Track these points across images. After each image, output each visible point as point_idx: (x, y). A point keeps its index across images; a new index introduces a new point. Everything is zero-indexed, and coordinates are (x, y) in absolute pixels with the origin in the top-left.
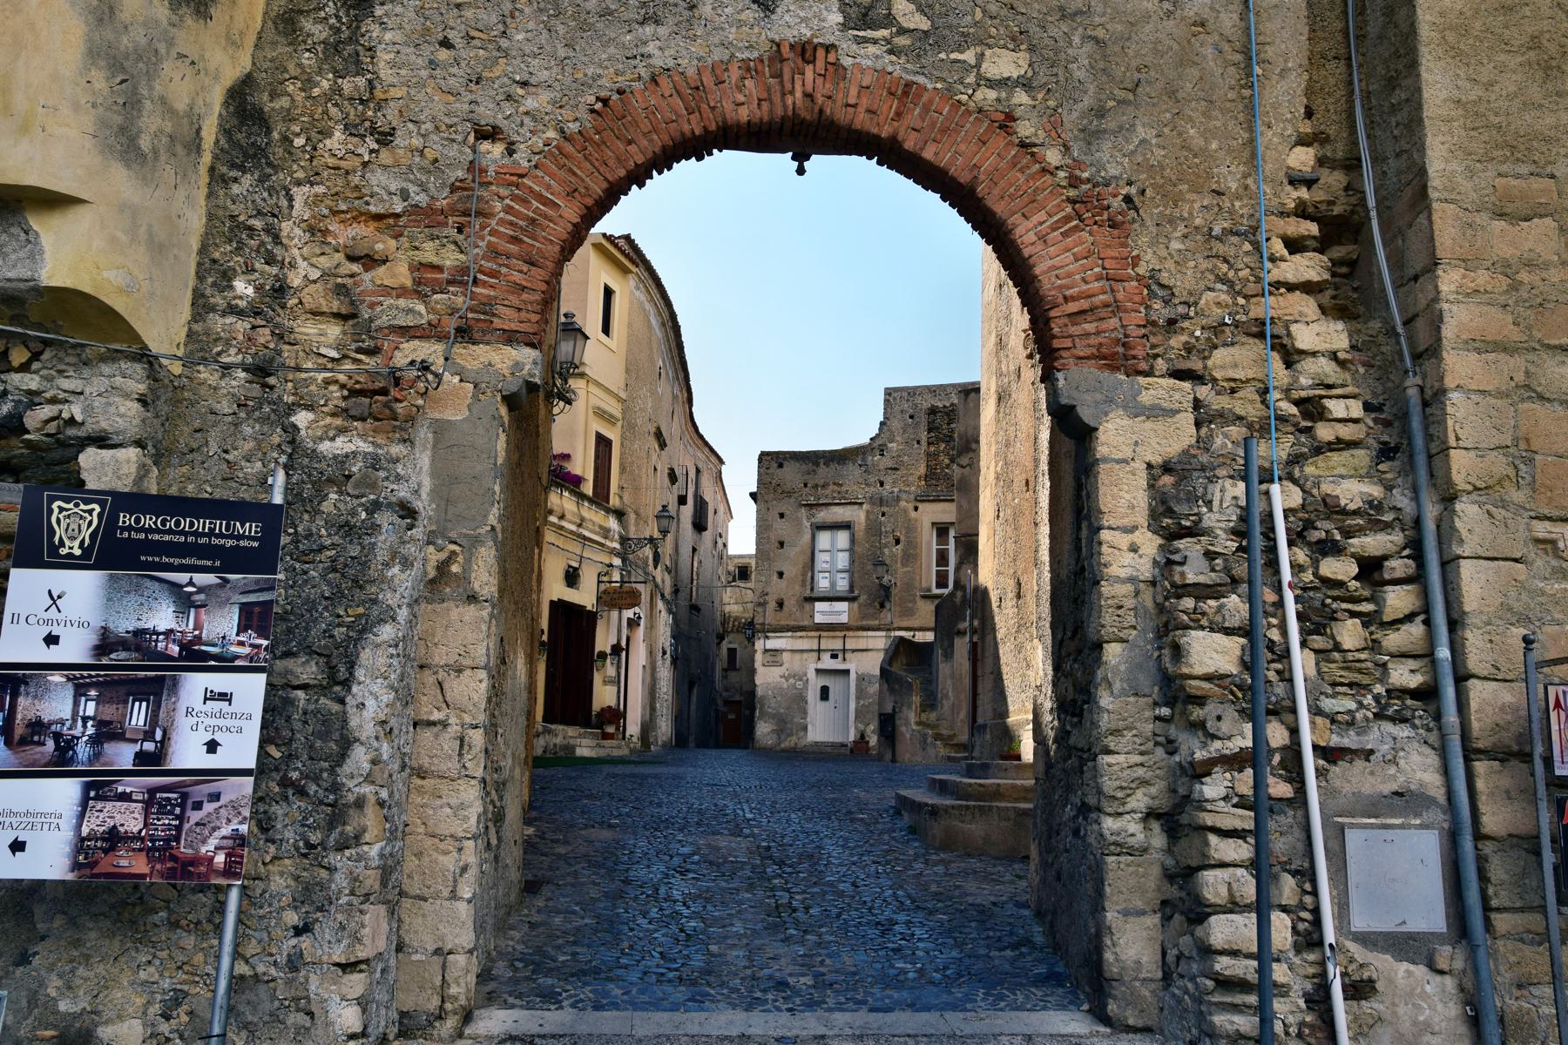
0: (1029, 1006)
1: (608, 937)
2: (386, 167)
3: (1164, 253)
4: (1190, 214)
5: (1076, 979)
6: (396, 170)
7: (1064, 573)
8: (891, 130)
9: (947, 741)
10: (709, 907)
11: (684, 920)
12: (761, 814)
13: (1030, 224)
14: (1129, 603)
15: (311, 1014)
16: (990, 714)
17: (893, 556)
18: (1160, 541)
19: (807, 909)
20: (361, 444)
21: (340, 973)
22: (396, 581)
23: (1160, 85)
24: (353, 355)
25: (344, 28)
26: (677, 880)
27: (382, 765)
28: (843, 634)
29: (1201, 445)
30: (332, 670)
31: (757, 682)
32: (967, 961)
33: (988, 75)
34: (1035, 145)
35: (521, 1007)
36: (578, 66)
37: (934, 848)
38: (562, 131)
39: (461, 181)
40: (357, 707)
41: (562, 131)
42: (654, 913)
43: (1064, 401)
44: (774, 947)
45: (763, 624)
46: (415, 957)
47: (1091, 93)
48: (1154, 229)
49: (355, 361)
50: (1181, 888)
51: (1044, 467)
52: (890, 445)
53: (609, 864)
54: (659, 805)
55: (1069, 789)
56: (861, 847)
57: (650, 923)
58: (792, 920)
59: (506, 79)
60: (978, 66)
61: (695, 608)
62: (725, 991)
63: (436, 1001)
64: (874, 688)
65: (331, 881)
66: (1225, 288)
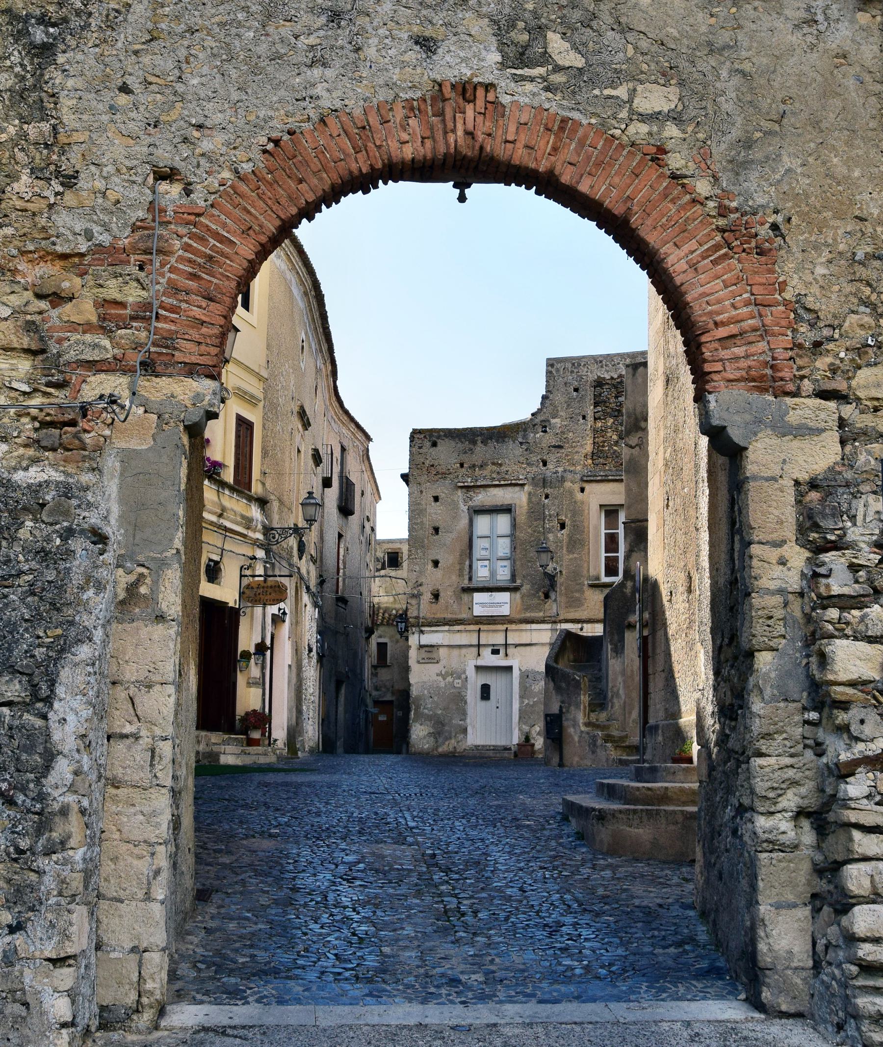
0: (689, 997)
1: (284, 941)
2: (70, 208)
3: (809, 278)
4: (835, 240)
5: (736, 972)
6: (80, 211)
7: (722, 581)
8: (549, 165)
9: (618, 742)
10: (379, 913)
11: (354, 925)
12: (424, 822)
13: (681, 253)
14: (779, 613)
15: (26, 1005)
16: (661, 714)
17: (558, 541)
18: (808, 554)
19: (475, 913)
20: (53, 473)
21: (52, 968)
22: (91, 603)
23: (804, 116)
24: (44, 389)
25: (29, 76)
26: (344, 887)
27: (83, 776)
28: (504, 627)
29: (846, 462)
30: (34, 688)
31: (412, 681)
32: (631, 958)
33: (640, 110)
34: (686, 177)
35: (210, 1003)
36: (250, 109)
37: (602, 854)
38: (237, 172)
39: (142, 220)
40: (59, 722)
41: (237, 172)
42: (325, 918)
43: (715, 422)
44: (445, 948)
45: (417, 618)
46: (113, 955)
47: (738, 125)
48: (799, 255)
49: (46, 394)
50: (829, 882)
51: (704, 474)
52: (553, 421)
53: (275, 872)
54: (318, 814)
55: (729, 791)
56: (528, 853)
57: (322, 927)
58: (461, 924)
59: (182, 122)
60: (630, 101)
61: (342, 600)
62: (401, 987)
63: (133, 996)
64: (539, 686)
65: (40, 883)
66: (868, 310)
